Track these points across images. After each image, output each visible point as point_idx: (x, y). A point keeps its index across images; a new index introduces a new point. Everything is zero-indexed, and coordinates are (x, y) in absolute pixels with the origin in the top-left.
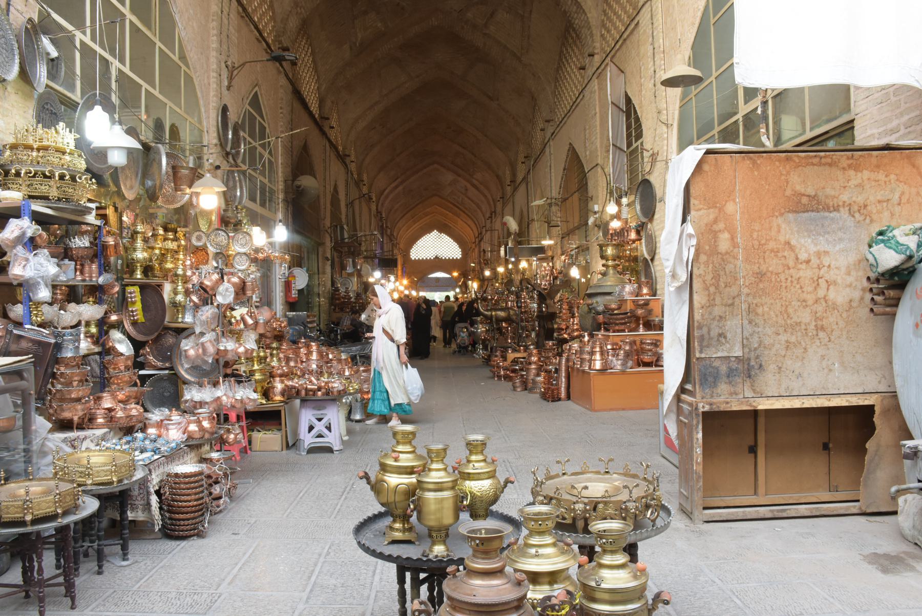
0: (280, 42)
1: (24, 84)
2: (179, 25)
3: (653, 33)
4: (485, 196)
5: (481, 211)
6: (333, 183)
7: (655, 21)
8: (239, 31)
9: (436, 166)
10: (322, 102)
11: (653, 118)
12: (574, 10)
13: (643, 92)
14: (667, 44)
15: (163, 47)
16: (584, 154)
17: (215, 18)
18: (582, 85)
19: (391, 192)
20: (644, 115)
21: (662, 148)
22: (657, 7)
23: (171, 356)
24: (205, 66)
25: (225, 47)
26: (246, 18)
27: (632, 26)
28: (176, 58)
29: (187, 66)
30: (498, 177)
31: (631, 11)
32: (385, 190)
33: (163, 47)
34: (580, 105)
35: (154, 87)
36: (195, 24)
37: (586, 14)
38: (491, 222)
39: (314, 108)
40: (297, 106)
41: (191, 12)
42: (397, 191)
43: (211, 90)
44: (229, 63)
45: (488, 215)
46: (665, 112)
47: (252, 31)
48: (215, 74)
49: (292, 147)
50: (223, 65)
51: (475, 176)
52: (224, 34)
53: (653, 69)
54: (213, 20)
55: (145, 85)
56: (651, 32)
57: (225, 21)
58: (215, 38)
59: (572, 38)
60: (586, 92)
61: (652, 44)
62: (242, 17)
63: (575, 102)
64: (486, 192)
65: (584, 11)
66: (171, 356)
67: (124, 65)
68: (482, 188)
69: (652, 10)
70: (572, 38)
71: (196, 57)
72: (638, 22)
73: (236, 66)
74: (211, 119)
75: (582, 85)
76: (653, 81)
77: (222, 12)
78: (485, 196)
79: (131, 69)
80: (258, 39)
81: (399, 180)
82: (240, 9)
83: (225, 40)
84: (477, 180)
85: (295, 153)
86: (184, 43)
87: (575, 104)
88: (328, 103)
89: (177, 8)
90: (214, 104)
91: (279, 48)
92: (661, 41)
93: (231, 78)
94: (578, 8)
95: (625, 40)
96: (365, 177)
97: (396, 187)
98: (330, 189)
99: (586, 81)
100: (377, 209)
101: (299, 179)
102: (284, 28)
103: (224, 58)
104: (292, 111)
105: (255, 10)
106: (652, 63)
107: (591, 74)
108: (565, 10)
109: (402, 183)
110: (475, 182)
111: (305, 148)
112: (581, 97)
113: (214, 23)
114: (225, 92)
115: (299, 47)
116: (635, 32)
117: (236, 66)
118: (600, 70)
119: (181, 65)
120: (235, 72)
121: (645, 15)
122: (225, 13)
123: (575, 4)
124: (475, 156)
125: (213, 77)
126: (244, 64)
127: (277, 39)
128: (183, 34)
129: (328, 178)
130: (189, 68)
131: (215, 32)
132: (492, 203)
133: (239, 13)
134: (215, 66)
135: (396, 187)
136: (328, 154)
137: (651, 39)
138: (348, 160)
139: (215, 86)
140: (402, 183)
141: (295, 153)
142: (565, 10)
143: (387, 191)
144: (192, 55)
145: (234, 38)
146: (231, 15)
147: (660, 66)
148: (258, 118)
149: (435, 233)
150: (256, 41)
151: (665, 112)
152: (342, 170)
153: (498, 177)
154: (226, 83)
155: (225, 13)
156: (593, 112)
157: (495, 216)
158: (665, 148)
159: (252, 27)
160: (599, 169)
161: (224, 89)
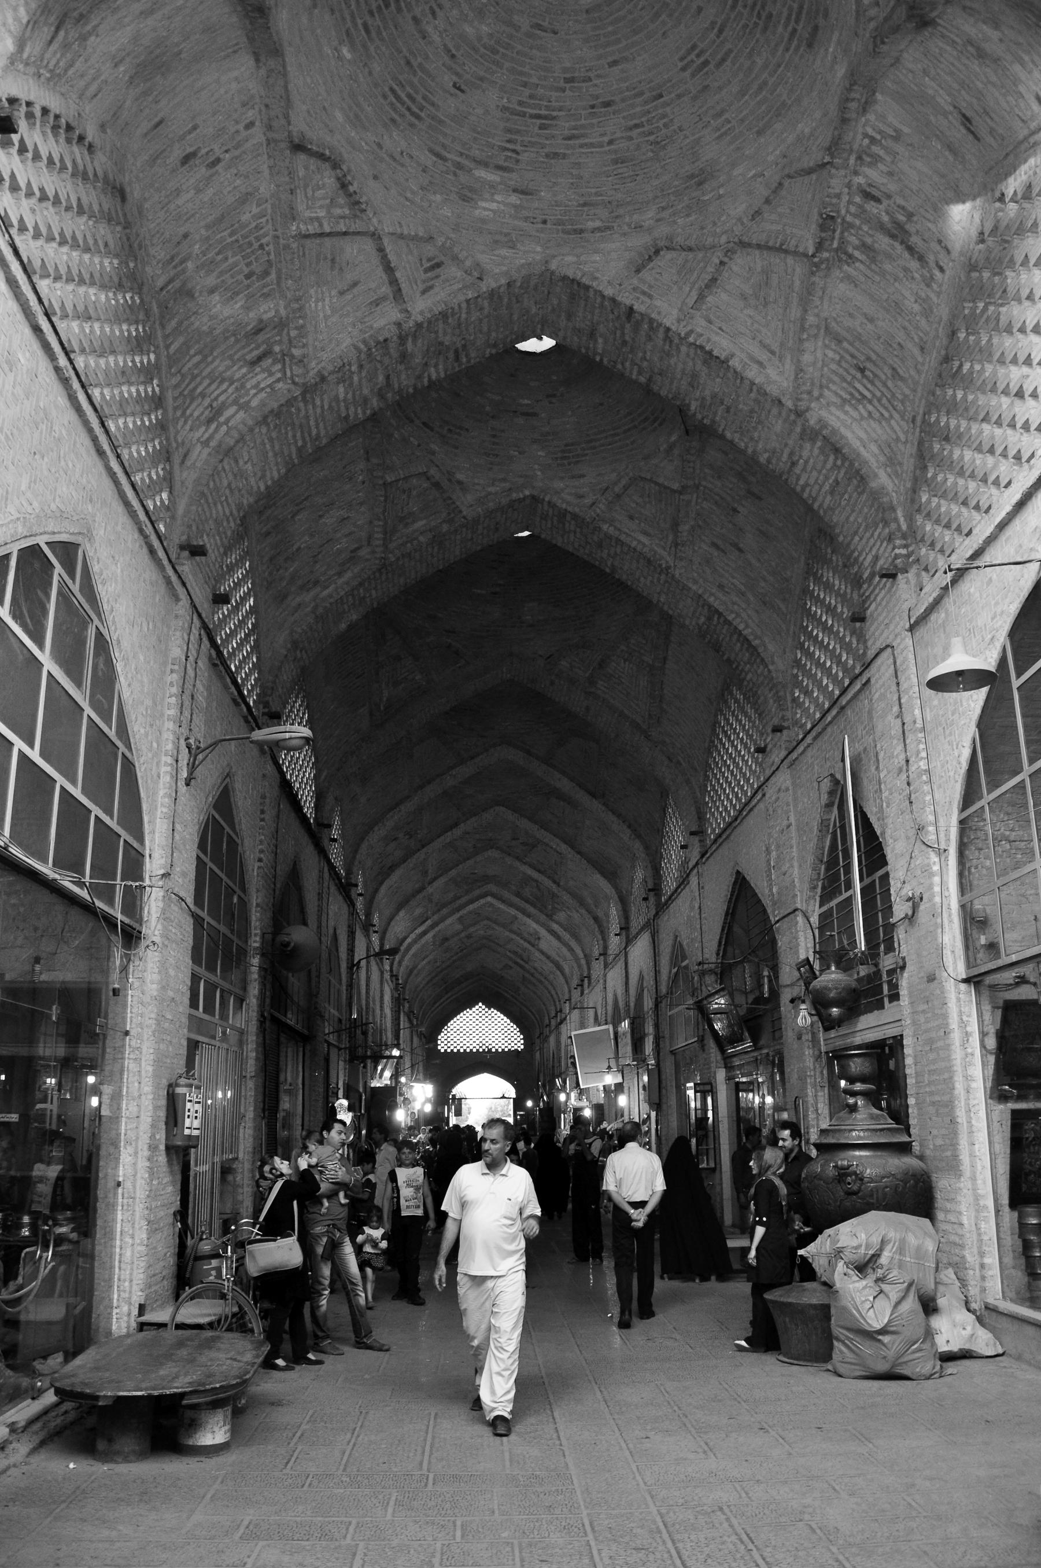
0: (266, 705)
1: (938, 1195)
2: (122, 679)
3: (899, 699)
4: (571, 950)
5: (563, 974)
6: (331, 931)
7: (902, 679)
8: (208, 689)
9: (489, 899)
10: (320, 797)
11: (908, 838)
12: (746, 659)
13: (885, 794)
14: (928, 717)
15: (94, 716)
16: (767, 891)
17: (176, 667)
18: (758, 778)
19: (415, 941)
20: (888, 832)
21: (931, 887)
22: (905, 659)
23: (276, 1367)
24: (155, 745)
25: (187, 713)
26: (221, 668)
27: (857, 686)
28: (112, 734)
29: (129, 746)
30: (596, 919)
31: (851, 662)
32: (405, 938)
33: (94, 716)
34: (756, 810)
35: (74, 782)
36: (145, 680)
37: (766, 666)
38: (582, 994)
39: (309, 809)
40: (285, 806)
41: (142, 658)
42: (423, 941)
43: (161, 786)
44: (192, 741)
45: (575, 982)
46: (931, 829)
47: (226, 687)
48: (169, 760)
49: (275, 877)
50: (183, 743)
51: (555, 917)
52: (188, 693)
53: (902, 756)
54: (172, 671)
55: (60, 780)
56: (896, 697)
57: (191, 672)
58: (173, 700)
59: (737, 701)
60: (770, 791)
61: (900, 715)
62: (215, 665)
63: (746, 804)
64: (573, 943)
65: (763, 660)
66: (276, 1367)
67: (31, 745)
68: (566, 936)
69: (895, 663)
70: (737, 701)
71: (142, 731)
72: (868, 681)
73: (202, 745)
74: (157, 835)
75: (758, 778)
76: (904, 776)
77: (187, 657)
78: (571, 950)
79: (42, 755)
80: (234, 701)
81: (429, 922)
82: (213, 653)
83: (187, 703)
84: (557, 923)
85: (278, 886)
86: (128, 708)
87: (748, 808)
88: (330, 799)
89: (120, 651)
90: (165, 810)
91: (264, 714)
92: (917, 712)
93: (192, 767)
94: (752, 655)
95: (843, 708)
96: (376, 920)
97: (425, 933)
98: (327, 941)
99: (768, 772)
100: (391, 970)
101: (286, 930)
102: (274, 682)
103: (184, 731)
104: (278, 816)
105: (232, 655)
106: (901, 747)
107: (777, 761)
108: (728, 660)
109: (432, 927)
110: (555, 927)
111: (294, 875)
112: (759, 796)
113: (174, 675)
114: (182, 788)
115: (291, 711)
116: (861, 697)
117: (202, 745)
118: (794, 755)
119: (118, 743)
120: (200, 757)
121: (883, 669)
122: (191, 659)
123: (747, 650)
124: (559, 885)
125: (166, 763)
126: (215, 744)
127: (261, 700)
128: (126, 694)
129: (324, 924)
130: (130, 749)
131: (174, 690)
132: (583, 962)
133: (210, 658)
134: (170, 746)
135: (425, 933)
136: (326, 884)
137: (896, 709)
138: (353, 893)
139: (168, 778)
140: (432, 927)
141: (278, 886)
142: (728, 660)
143: (409, 940)
144: (137, 728)
145: (200, 698)
146: (200, 663)
147: (918, 752)
148: (227, 829)
149: (479, 1008)
150: (232, 704)
151: (931, 829)
152: (345, 909)
153: (596, 919)
154: (185, 775)
155: (191, 659)
156: (785, 823)
157: (589, 983)
158: (937, 889)
159: (228, 680)
160: (800, 919)
161: (181, 784)
